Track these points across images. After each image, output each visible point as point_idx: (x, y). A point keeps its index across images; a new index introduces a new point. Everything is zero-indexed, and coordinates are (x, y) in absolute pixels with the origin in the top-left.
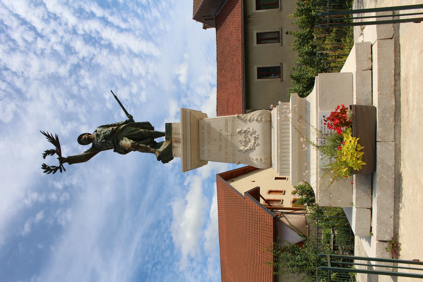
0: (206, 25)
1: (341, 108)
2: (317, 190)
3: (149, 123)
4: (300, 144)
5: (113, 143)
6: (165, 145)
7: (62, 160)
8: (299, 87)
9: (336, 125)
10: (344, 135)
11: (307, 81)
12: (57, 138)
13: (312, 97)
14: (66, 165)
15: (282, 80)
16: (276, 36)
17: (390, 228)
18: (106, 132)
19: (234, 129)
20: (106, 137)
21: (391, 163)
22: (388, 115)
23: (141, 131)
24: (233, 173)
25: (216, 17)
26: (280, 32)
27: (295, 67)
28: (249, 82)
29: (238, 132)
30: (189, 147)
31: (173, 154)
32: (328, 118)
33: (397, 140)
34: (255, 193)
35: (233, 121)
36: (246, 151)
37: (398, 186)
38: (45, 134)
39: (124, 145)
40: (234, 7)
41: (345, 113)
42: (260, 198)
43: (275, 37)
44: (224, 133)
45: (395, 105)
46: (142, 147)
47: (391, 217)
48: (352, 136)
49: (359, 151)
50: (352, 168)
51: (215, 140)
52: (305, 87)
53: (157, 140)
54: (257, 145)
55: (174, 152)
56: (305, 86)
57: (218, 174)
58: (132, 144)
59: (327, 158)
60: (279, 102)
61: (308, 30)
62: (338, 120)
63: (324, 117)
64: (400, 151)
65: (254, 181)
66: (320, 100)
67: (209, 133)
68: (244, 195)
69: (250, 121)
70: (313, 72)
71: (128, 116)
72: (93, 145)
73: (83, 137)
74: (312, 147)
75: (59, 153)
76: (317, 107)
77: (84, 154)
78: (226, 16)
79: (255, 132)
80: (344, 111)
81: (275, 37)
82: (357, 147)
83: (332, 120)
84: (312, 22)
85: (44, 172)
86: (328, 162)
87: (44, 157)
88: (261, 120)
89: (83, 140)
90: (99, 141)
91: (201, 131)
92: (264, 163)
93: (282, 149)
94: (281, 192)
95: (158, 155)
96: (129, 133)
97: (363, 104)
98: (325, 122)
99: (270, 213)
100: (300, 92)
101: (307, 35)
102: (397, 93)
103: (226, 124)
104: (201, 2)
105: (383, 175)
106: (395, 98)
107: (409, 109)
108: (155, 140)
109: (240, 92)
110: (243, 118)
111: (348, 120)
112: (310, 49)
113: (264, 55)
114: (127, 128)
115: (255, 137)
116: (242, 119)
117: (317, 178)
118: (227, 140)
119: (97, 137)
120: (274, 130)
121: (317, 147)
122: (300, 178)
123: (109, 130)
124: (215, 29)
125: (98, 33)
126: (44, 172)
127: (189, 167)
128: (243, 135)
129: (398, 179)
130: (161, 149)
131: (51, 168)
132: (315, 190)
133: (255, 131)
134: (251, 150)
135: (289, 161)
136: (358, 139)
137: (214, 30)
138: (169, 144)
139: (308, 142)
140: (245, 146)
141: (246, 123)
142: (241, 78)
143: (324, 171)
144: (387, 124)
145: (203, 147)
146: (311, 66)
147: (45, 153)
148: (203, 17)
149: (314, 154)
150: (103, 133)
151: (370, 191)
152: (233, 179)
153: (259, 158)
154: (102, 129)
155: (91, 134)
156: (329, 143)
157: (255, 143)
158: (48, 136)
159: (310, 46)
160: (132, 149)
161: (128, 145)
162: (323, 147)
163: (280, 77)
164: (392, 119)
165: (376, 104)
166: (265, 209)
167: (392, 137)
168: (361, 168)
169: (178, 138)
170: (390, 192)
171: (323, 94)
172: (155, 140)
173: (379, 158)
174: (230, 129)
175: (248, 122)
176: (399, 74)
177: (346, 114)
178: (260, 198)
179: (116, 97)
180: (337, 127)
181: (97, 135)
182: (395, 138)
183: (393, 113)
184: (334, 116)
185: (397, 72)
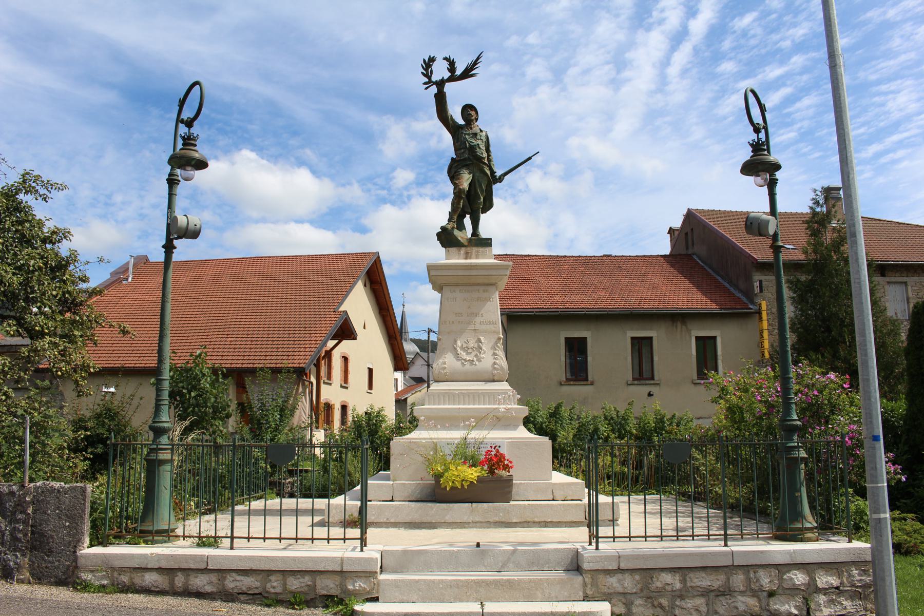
0: (676, 233)
4: (465, 419)
5: (465, 160)
7: (441, 84)
8: (542, 416)
9: (491, 459)
10: (479, 468)
12: (472, 76)
13: (522, 433)
14: (434, 89)
15: (561, 384)
19: (484, 332)
20: (473, 149)
21: (448, 518)
25: (689, 256)
26: (652, 382)
28: (560, 320)
30: (461, 273)
32: (498, 451)
34: (345, 332)
36: (455, 349)
38: (478, 58)
40: (704, 294)
41: (504, 469)
43: (643, 369)
44: (478, 320)
46: (459, 203)
50: (442, 477)
53: (467, 221)
55: (453, 250)
56: (544, 426)
58: (464, 189)
59: (448, 450)
61: (634, 432)
62: (495, 462)
67: (478, 299)
68: (341, 309)
69: (495, 354)
70: (566, 439)
72: (461, 127)
73: (473, 113)
78: (690, 277)
79: (479, 360)
81: (643, 369)
83: (496, 455)
84: (644, 437)
85: (424, 60)
86: (448, 452)
87: (445, 59)
88: (495, 368)
89: (469, 111)
94: (346, 380)
95: (449, 227)
100: (535, 418)
101: (625, 429)
102: (525, 524)
103: (490, 323)
104: (719, 227)
108: (468, 216)
109: (541, 305)
113: (609, 350)
116: (496, 343)
117: (424, 439)
118: (469, 323)
122: (429, 419)
124: (667, 251)
125: (661, 22)
126: (424, 60)
127: (433, 273)
128: (476, 345)
134: (457, 356)
137: (666, 249)
140: (462, 348)
142: (567, 305)
143: (435, 446)
146: (575, 436)
149: (456, 435)
152: (368, 285)
154: (485, 140)
156: (469, 452)
157: (465, 360)
158: (475, 63)
164: (497, 519)
165: (512, 503)
168: (443, 486)
172: (468, 216)
174: (484, 327)
175: (492, 352)
179: (530, 158)
180: (489, 460)
181: (475, 135)
183: (503, 520)
184: (500, 457)
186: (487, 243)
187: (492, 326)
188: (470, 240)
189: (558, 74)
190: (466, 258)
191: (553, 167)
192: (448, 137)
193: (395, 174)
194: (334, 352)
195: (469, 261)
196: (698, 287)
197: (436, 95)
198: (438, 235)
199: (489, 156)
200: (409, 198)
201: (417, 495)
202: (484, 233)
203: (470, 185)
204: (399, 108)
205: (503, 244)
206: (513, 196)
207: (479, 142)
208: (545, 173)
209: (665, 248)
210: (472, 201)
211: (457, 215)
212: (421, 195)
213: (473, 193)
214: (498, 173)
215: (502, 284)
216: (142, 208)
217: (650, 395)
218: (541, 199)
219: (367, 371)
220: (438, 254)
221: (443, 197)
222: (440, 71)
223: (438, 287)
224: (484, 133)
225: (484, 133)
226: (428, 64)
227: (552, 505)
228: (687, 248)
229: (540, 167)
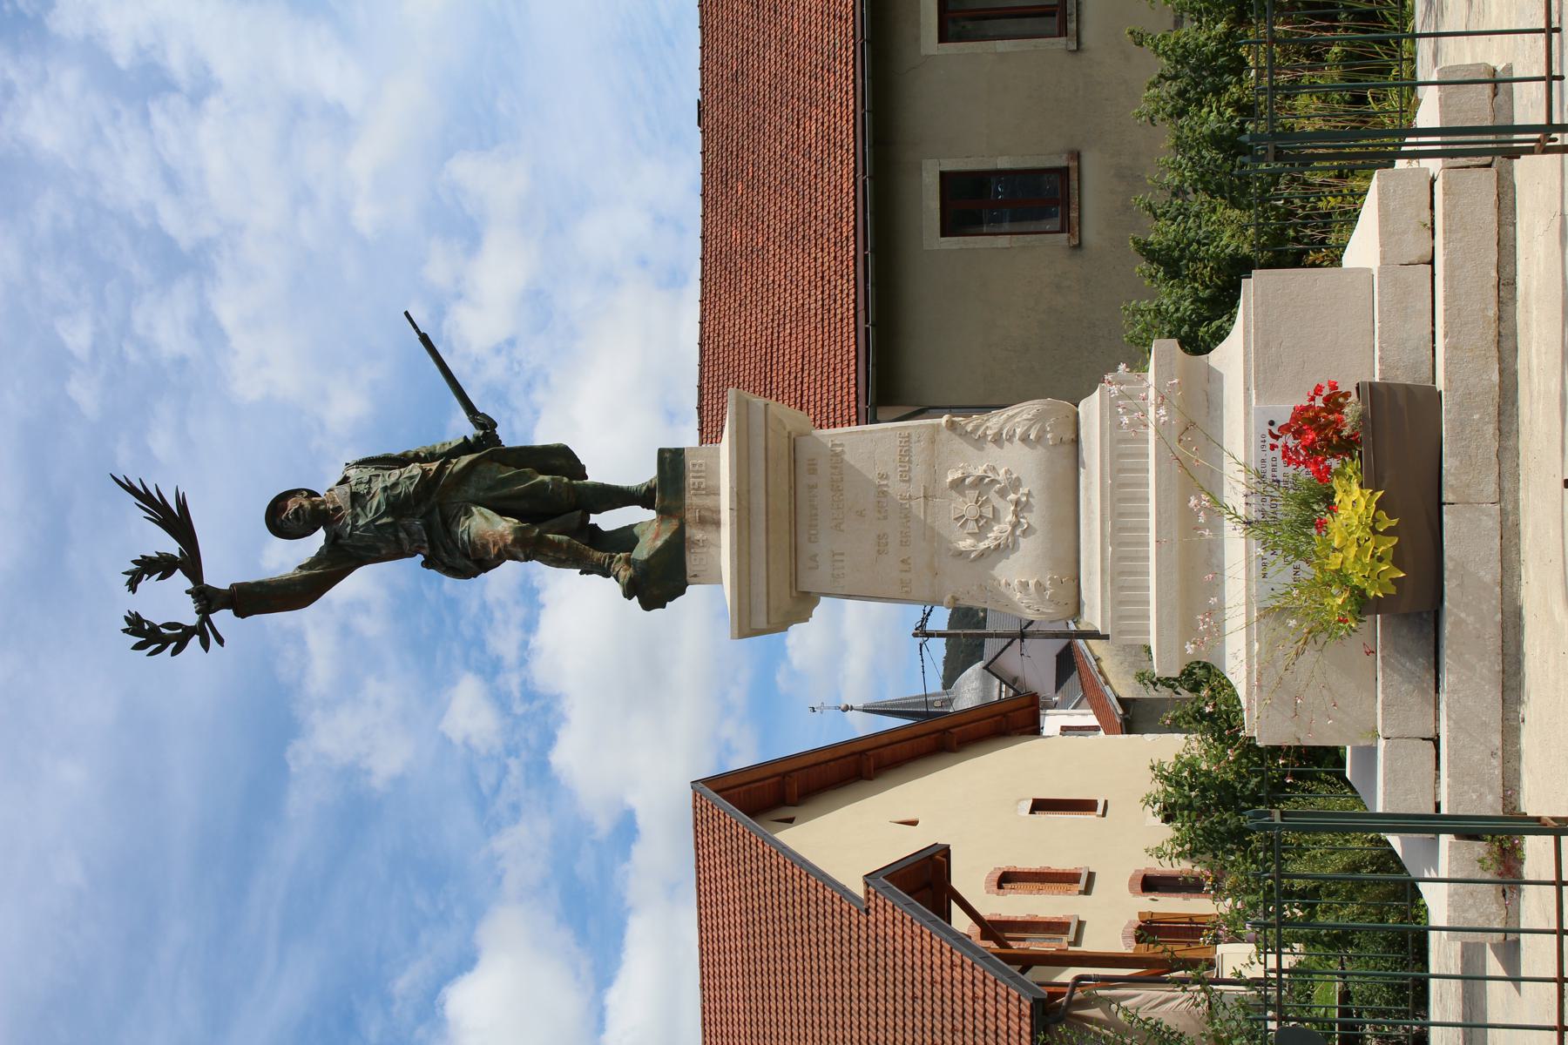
1: (1326, 392)
2: (1249, 693)
3: (566, 448)
4: (1188, 515)
5: (428, 528)
6: (657, 536)
7: (207, 599)
8: (1175, 299)
9: (1310, 448)
10: (1336, 483)
11: (1217, 271)
12: (182, 506)
13: (1230, 356)
14: (223, 619)
15: (1079, 246)
17: (1491, 789)
18: (395, 485)
19: (934, 472)
20: (397, 505)
21: (1489, 573)
22: (1476, 417)
23: (543, 483)
24: (785, 775)
27: (1160, 199)
29: (953, 482)
30: (760, 540)
31: (690, 571)
32: (1285, 429)
33: (1508, 497)
34: (925, 879)
35: (933, 441)
36: (982, 555)
37: (1512, 650)
38: (131, 490)
39: (482, 537)
42: (954, 907)
44: (896, 488)
45: (1501, 382)
46: (556, 546)
47: (1493, 754)
48: (1361, 486)
49: (1383, 534)
50: (1363, 593)
51: (861, 514)
52: (1203, 301)
53: (608, 521)
54: (1024, 532)
55: (692, 562)
57: (706, 781)
58: (516, 530)
60: (1122, 367)
61: (1221, 27)
62: (1317, 434)
63: (1272, 423)
64: (1518, 535)
65: (914, 823)
66: (1257, 366)
67: (836, 488)
68: (859, 890)
69: (998, 440)
70: (1243, 228)
71: (473, 420)
72: (332, 540)
73: (292, 505)
74: (1228, 525)
76: (1247, 390)
77: (299, 574)
79: (1016, 484)
80: (1335, 401)
82: (1375, 520)
83: (1298, 434)
85: (138, 647)
87: (133, 586)
88: (1039, 438)
89: (286, 517)
90: (361, 522)
91: (804, 479)
92: (1051, 600)
93: (1120, 544)
95: (625, 574)
96: (490, 488)
97: (1403, 378)
98: (1274, 441)
99: (1013, 977)
100: (1182, 321)
101: (1215, 56)
102: (1507, 344)
103: (905, 454)
105: (1463, 615)
106: (1501, 360)
107: (1531, 393)
108: (594, 519)
110: (969, 428)
111: (1346, 432)
112: (1231, 119)
114: (480, 468)
115: (1017, 503)
116: (965, 435)
118: (906, 515)
119: (353, 506)
120: (1088, 476)
121: (1248, 523)
123: (411, 478)
126: (138, 647)
127: (760, 621)
128: (973, 494)
129: (1512, 624)
130: (642, 552)
131: (163, 630)
132: (1241, 692)
133: (1018, 479)
134: (1003, 550)
135: (1148, 588)
136: (1380, 494)
138: (674, 533)
139: (1217, 506)
140: (980, 535)
141: (981, 449)
142: (848, 230)
143: (1271, 613)
144: (1474, 445)
145: (810, 540)
146: (1234, 204)
147: (134, 567)
149: (1236, 549)
150: (385, 489)
151: (1430, 678)
153: (1032, 583)
154: (371, 471)
155: (318, 495)
156: (1287, 512)
157: (1015, 526)
159: (1228, 105)
161: (502, 536)
162: (1267, 524)
163: (1065, 228)
164: (1490, 429)
165: (1440, 384)
166: (985, 958)
167: (1491, 488)
168: (1392, 591)
169: (708, 509)
170: (1488, 668)
171: (1267, 345)
172: (594, 519)
173: (1452, 559)
174: (919, 471)
176: (1513, 283)
177: (1340, 412)
178: (954, 907)
179: (425, 339)
180: (1313, 455)
181: (356, 498)
182: (1501, 492)
183: (1493, 410)
185: (1504, 276)
186: (671, 462)
188: (664, 513)
189: (183, 264)
190: (717, 524)
191: (438, 271)
192: (360, 583)
193: (457, 737)
195: (726, 516)
198: (648, 605)
199: (417, 458)
200: (529, 695)
202: (643, 473)
203: (502, 512)
204: (273, 721)
205: (671, 416)
206: (529, 386)
207: (378, 485)
208: (459, 296)
210: (552, 507)
211: (590, 551)
212: (523, 662)
215: (789, 416)
218: (537, 303)
220: (703, 608)
221: (530, 597)
222: (169, 601)
223: (800, 605)
224: (352, 473)
225: (352, 473)
226: (147, 635)
229: (440, 312)
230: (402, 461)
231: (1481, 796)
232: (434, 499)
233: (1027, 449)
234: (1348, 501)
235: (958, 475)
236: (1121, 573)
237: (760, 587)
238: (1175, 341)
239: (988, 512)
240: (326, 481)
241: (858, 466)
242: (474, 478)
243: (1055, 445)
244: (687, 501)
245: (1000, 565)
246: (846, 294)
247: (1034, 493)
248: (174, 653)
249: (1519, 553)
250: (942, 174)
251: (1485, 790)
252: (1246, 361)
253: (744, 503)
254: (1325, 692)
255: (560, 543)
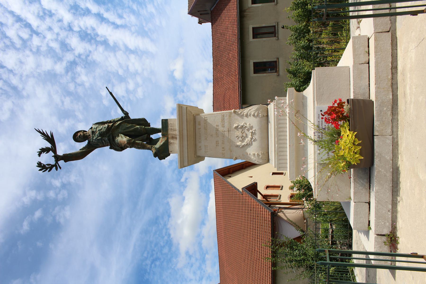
0: (201, 20)
1: (338, 102)
4: (298, 140)
5: (109, 139)
7: (57, 158)
10: (342, 129)
11: (304, 75)
12: (52, 135)
13: (309, 92)
14: (61, 163)
15: (279, 75)
16: (272, 30)
17: (388, 222)
18: (101, 129)
19: (230, 124)
20: (102, 134)
21: (389, 157)
22: (385, 109)
23: (137, 128)
25: (212, 12)
26: (276, 26)
27: (291, 61)
30: (185, 143)
31: (170, 150)
32: (326, 113)
33: (395, 133)
34: (253, 189)
35: (230, 116)
36: (243, 146)
37: (395, 180)
38: (40, 132)
39: (120, 142)
42: (258, 193)
43: (271, 32)
44: (221, 129)
47: (389, 211)
48: (349, 130)
49: (357, 145)
50: (350, 162)
51: (212, 136)
52: (301, 82)
55: (171, 148)
56: (302, 80)
57: (216, 170)
59: (324, 152)
61: (304, 23)
62: (335, 114)
63: (321, 111)
64: (398, 145)
65: (252, 177)
67: (205, 129)
68: (241, 190)
69: (247, 116)
70: (310, 66)
72: (89, 142)
73: (79, 134)
75: (55, 151)
76: (314, 101)
78: (222, 10)
79: (252, 128)
80: (341, 105)
81: (271, 32)
82: (354, 141)
83: (329, 114)
85: (40, 170)
86: (326, 157)
87: (39, 155)
88: (258, 115)
89: (78, 137)
90: (94, 138)
91: (198, 127)
93: (279, 144)
94: (278, 187)
95: (154, 151)
96: (124, 129)
97: (360, 98)
98: (322, 117)
99: (268, 208)
100: (297, 86)
101: (303, 29)
102: (395, 87)
103: (223, 120)
105: (380, 169)
106: (393, 91)
109: (237, 87)
110: (239, 113)
111: (345, 114)
112: (307, 43)
113: (260, 50)
114: (122, 124)
115: (252, 133)
116: (238, 115)
117: (315, 173)
118: (224, 136)
121: (315, 141)
123: (105, 127)
125: (94, 29)
126: (40, 170)
127: (186, 163)
129: (396, 172)
130: (158, 145)
133: (252, 126)
134: (249, 145)
136: (356, 133)
137: (209, 24)
139: (305, 136)
140: (242, 141)
141: (243, 118)
142: (237, 73)
143: (322, 166)
144: (384, 118)
146: (308, 61)
148: (198, 11)
149: (311, 148)
150: (99, 130)
151: (367, 185)
152: (230, 175)
153: (256, 154)
154: (97, 126)
155: (86, 132)
156: (326, 138)
157: (252, 139)
158: (43, 134)
160: (128, 145)
161: (124, 142)
162: (321, 141)
164: (389, 113)
165: (373, 97)
166: (263, 204)
167: (389, 131)
168: (359, 162)
170: (388, 186)
171: (319, 89)
173: (377, 152)
174: (226, 124)
175: (245, 117)
176: (396, 68)
177: (343, 108)
178: (258, 193)
179: (111, 93)
180: (335, 121)
181: (93, 132)
182: (393, 132)
183: (390, 107)
184: (331, 111)
185: (394, 65)
187: (226, 118)
194: (263, 193)
196: (226, 5)
197: (65, 161)
201: (365, 182)
209: (208, 25)
213: (133, 133)
214: (121, 115)
216: (196, 280)
217: (283, 28)
219: (274, 176)
227: (377, 63)
228: (208, 14)
230: (103, 123)
231: (385, 223)
232: (110, 133)
233: (254, 118)
234: (346, 135)
235: (237, 125)
236: (280, 152)
237: (186, 155)
238: (294, 88)
239: (244, 135)
240: (87, 129)
241: (211, 123)
242: (121, 127)
243: (262, 117)
244: (169, 133)
245: (247, 149)
246: (237, 84)
247: (256, 130)
248: (49, 171)
249: (398, 150)
250: (254, 63)
251: (386, 221)
252: (314, 93)
253: (181, 133)
254: (336, 186)
255: (139, 143)
